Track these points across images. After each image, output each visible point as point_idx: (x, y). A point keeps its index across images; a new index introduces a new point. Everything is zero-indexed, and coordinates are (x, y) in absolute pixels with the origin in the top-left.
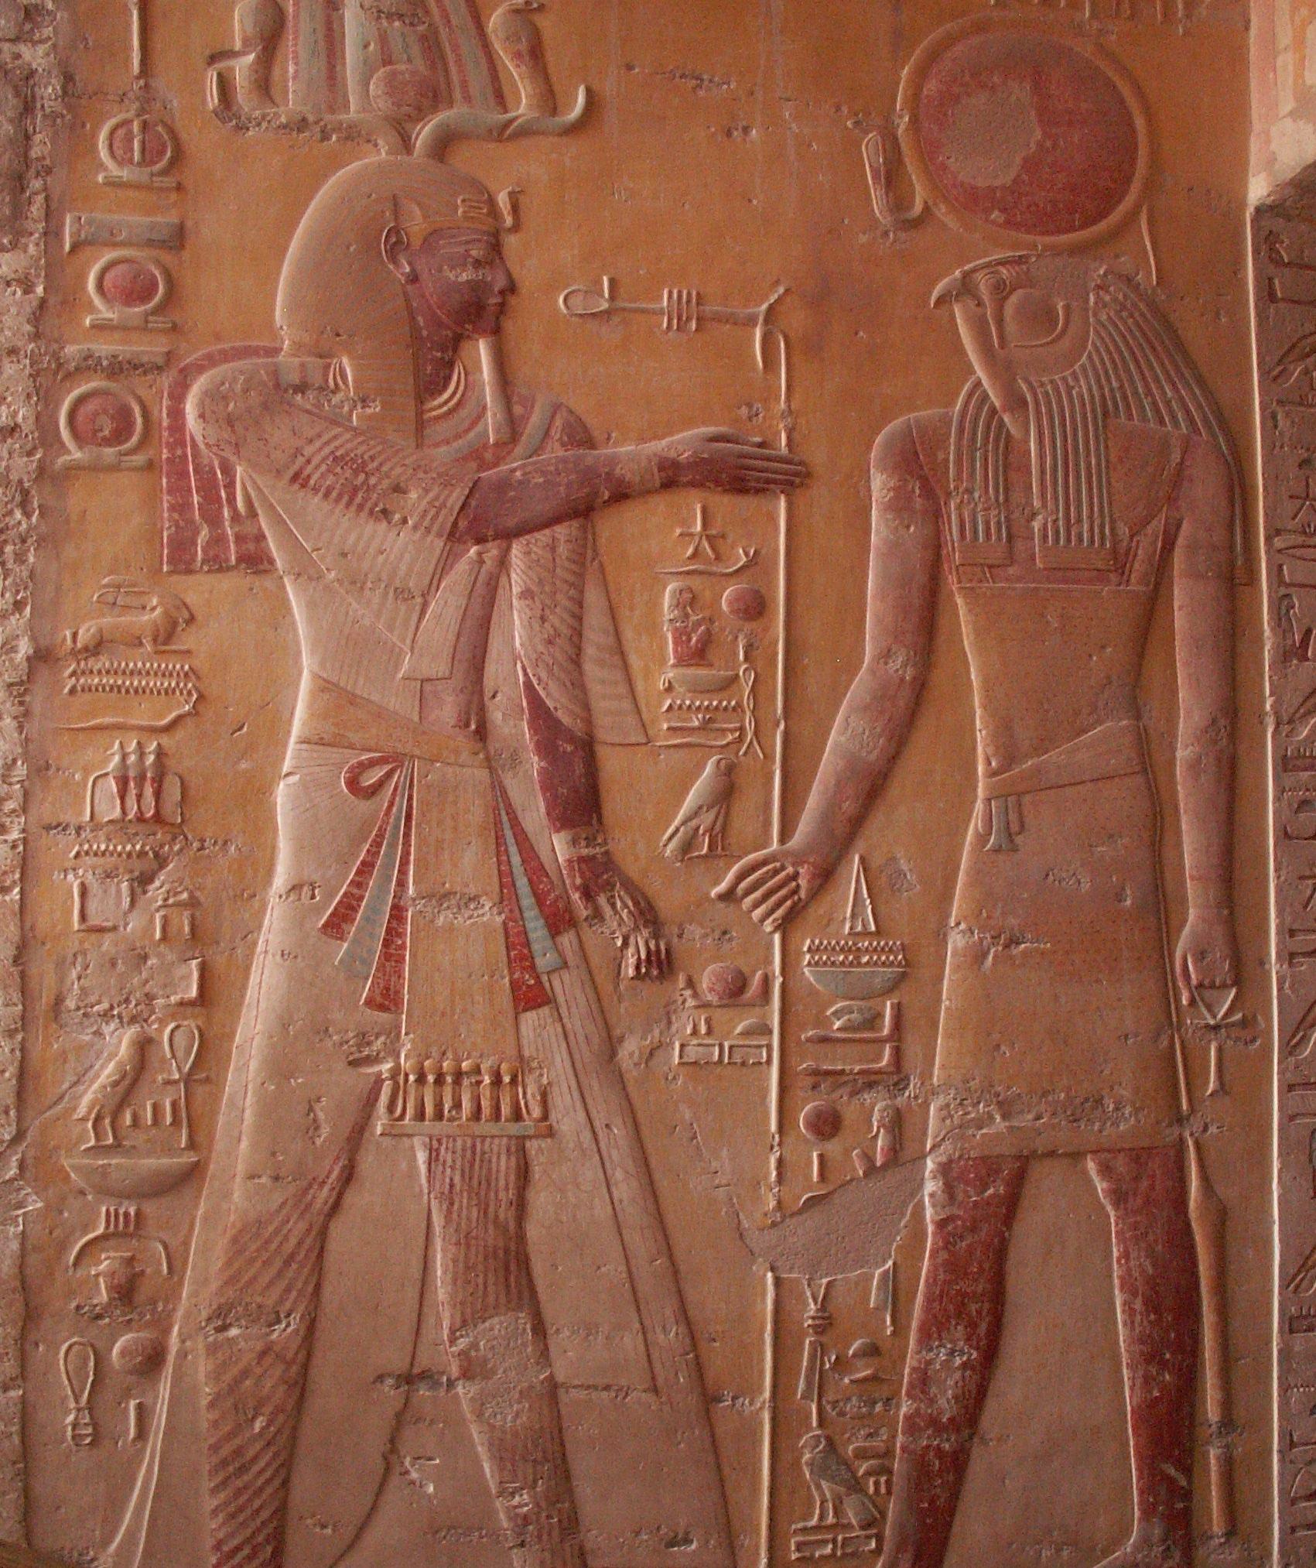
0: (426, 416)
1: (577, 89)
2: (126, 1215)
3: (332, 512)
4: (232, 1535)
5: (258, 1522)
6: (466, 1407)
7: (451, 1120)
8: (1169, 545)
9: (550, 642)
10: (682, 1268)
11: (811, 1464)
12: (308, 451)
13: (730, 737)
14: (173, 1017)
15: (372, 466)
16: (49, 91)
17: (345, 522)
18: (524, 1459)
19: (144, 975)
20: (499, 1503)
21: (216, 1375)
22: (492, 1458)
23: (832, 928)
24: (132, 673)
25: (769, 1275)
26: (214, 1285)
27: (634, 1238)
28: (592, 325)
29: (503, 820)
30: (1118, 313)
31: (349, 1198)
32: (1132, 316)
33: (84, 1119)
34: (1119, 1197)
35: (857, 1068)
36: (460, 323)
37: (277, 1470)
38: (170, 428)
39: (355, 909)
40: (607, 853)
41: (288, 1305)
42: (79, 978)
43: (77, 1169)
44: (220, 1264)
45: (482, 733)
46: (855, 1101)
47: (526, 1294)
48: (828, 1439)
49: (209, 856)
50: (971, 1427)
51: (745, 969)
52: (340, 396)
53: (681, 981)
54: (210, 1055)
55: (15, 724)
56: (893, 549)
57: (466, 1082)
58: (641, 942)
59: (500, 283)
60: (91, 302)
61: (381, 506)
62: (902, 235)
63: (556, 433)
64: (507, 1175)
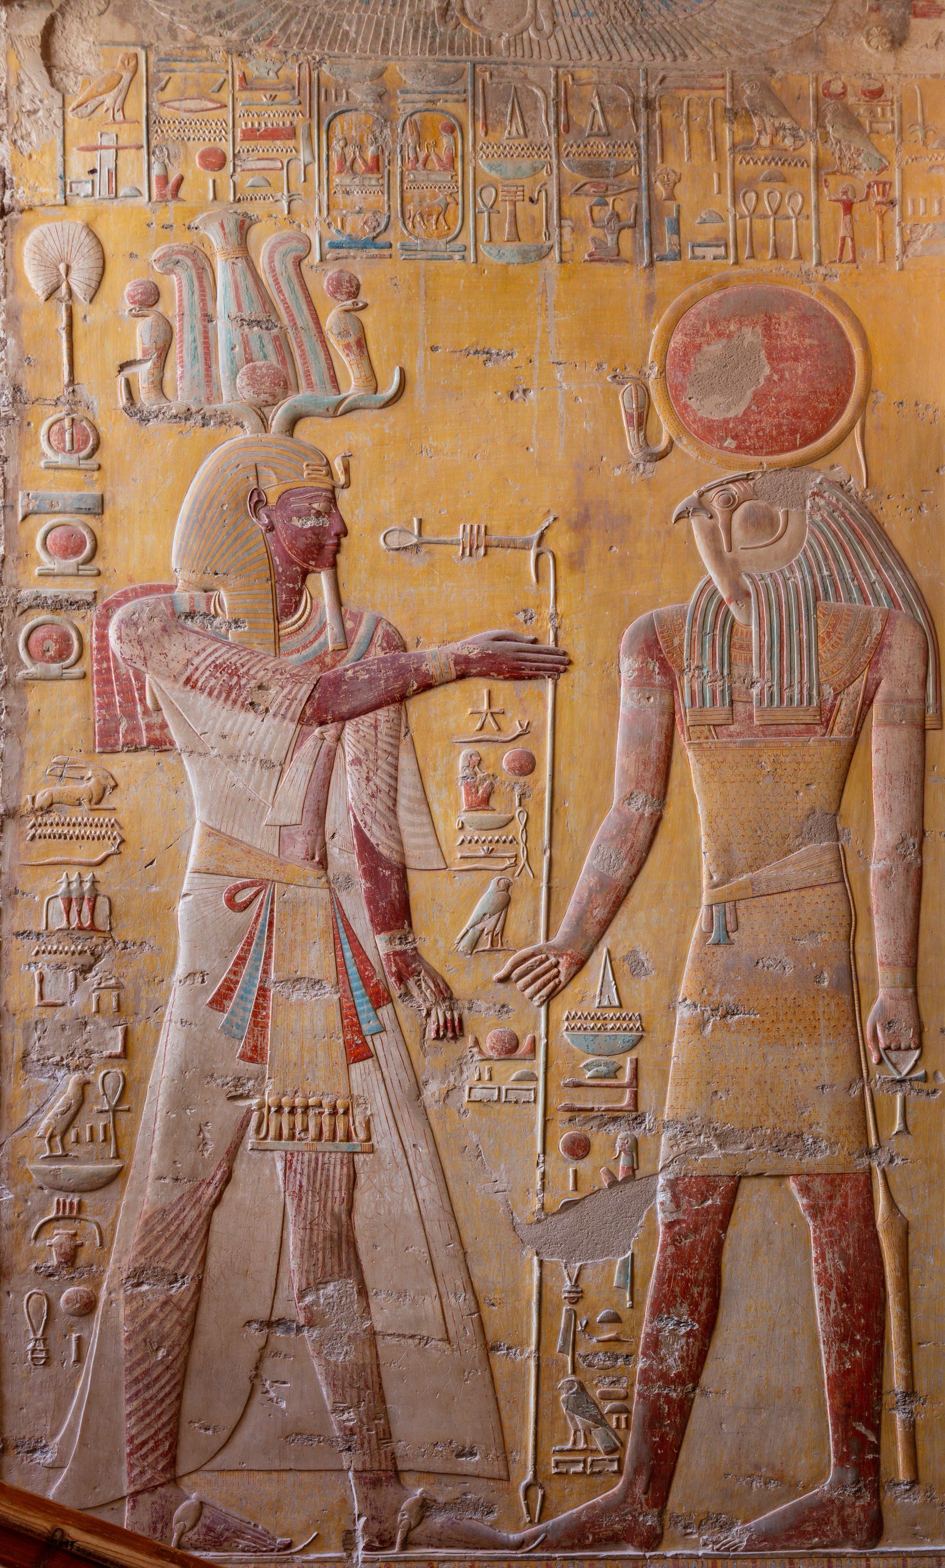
0: (282, 632)
1: (393, 370)
2: (71, 1204)
3: (214, 705)
4: (139, 1433)
6: (310, 1346)
7: (300, 1140)
8: (868, 702)
9: (373, 796)
10: (469, 1250)
11: (567, 1401)
13: (508, 863)
14: (105, 1065)
15: (242, 671)
17: (224, 713)
19: (85, 1037)
20: (333, 1417)
21: (132, 1317)
22: (328, 1384)
23: (584, 1004)
24: (74, 825)
25: (535, 1258)
26: (132, 1255)
27: (433, 1228)
28: (405, 556)
29: (340, 927)
30: (831, 515)
31: (226, 1195)
33: (42, 1137)
34: (816, 1211)
35: (604, 1107)
36: (306, 561)
37: (174, 1387)
38: (98, 649)
40: (415, 949)
41: (183, 1270)
43: (37, 1171)
44: (137, 1238)
45: (323, 863)
46: (602, 1132)
47: (353, 1267)
48: (580, 1383)
53: (470, 1040)
54: (127, 1095)
56: (637, 714)
57: (311, 1112)
58: (440, 1013)
59: (337, 528)
60: (38, 558)
61: (249, 700)
63: (378, 639)
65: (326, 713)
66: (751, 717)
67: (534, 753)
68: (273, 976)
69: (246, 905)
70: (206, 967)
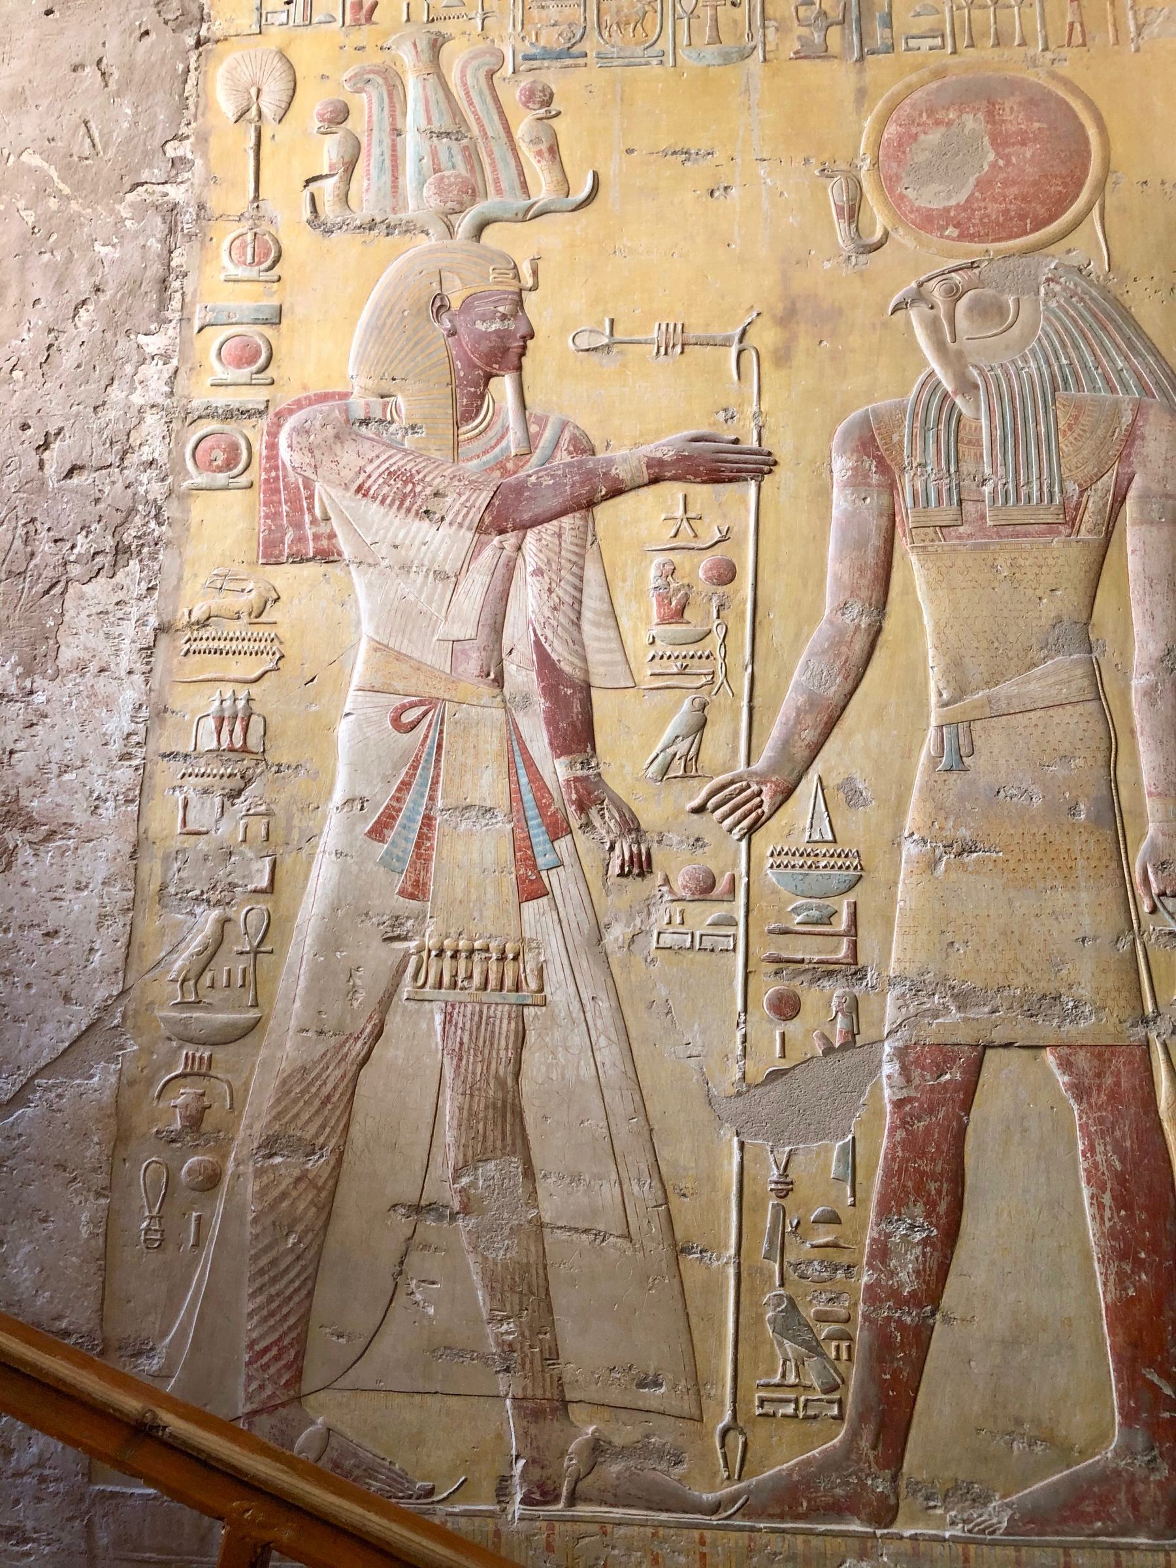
2: (201, 1058)
4: (262, 1337)
5: (285, 1327)
8: (1120, 499)
9: (555, 609)
11: (773, 1321)
12: (369, 469)
13: (704, 680)
16: (187, 220)
17: (397, 522)
18: (512, 1289)
20: (489, 1329)
21: (262, 1193)
22: (485, 1286)
25: (736, 1139)
29: (516, 749)
32: (1082, 300)
33: (174, 981)
34: (1080, 1091)
39: (394, 818)
41: (322, 1139)
42: (179, 870)
43: (165, 1020)
45: (499, 681)
48: (791, 1300)
49: (284, 778)
50: (933, 1303)
51: (716, 872)
52: (394, 426)
55: (142, 678)
56: (851, 516)
58: (624, 847)
59: (522, 331)
61: (424, 509)
62: (862, 258)
64: (507, 1037)
65: (507, 520)
66: (983, 517)
67: (735, 561)
68: (440, 804)
69: (413, 726)
70: (366, 793)
